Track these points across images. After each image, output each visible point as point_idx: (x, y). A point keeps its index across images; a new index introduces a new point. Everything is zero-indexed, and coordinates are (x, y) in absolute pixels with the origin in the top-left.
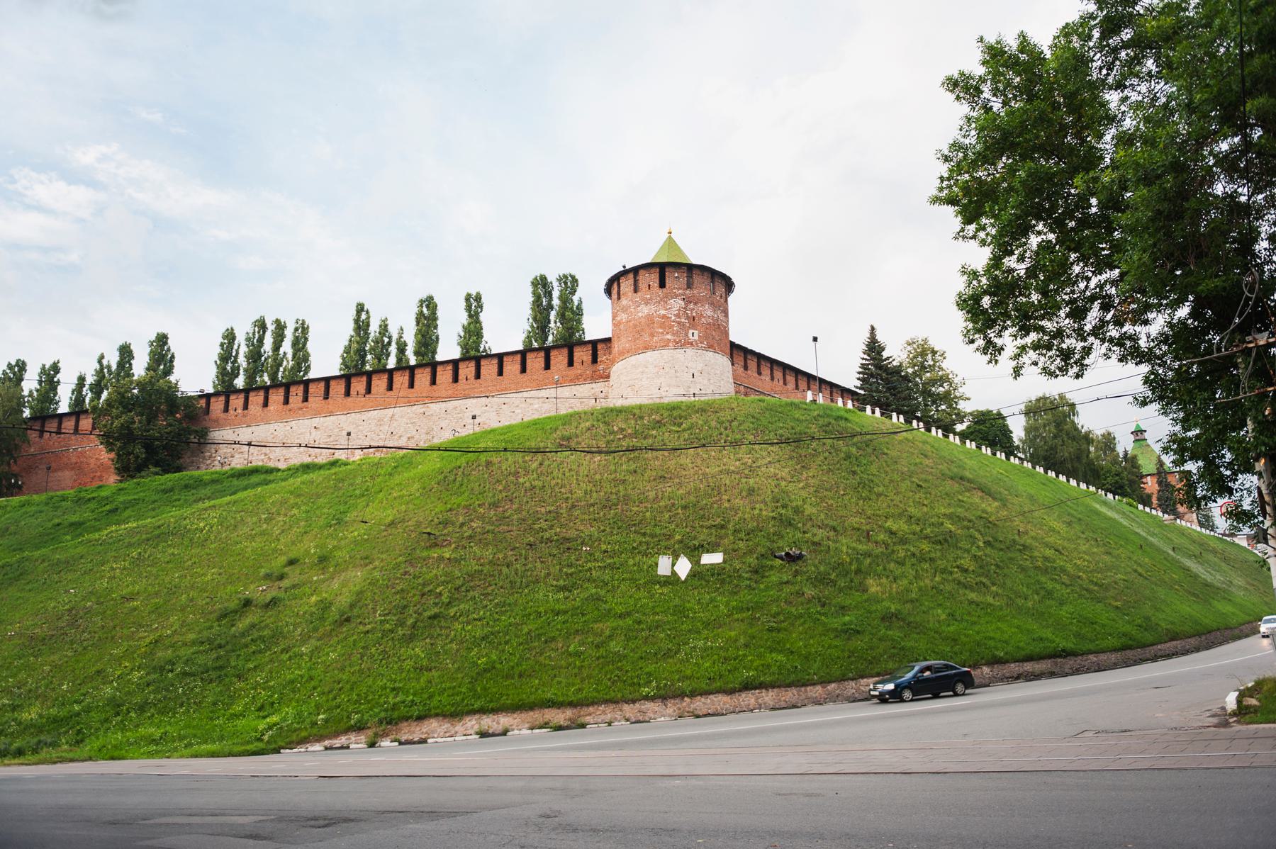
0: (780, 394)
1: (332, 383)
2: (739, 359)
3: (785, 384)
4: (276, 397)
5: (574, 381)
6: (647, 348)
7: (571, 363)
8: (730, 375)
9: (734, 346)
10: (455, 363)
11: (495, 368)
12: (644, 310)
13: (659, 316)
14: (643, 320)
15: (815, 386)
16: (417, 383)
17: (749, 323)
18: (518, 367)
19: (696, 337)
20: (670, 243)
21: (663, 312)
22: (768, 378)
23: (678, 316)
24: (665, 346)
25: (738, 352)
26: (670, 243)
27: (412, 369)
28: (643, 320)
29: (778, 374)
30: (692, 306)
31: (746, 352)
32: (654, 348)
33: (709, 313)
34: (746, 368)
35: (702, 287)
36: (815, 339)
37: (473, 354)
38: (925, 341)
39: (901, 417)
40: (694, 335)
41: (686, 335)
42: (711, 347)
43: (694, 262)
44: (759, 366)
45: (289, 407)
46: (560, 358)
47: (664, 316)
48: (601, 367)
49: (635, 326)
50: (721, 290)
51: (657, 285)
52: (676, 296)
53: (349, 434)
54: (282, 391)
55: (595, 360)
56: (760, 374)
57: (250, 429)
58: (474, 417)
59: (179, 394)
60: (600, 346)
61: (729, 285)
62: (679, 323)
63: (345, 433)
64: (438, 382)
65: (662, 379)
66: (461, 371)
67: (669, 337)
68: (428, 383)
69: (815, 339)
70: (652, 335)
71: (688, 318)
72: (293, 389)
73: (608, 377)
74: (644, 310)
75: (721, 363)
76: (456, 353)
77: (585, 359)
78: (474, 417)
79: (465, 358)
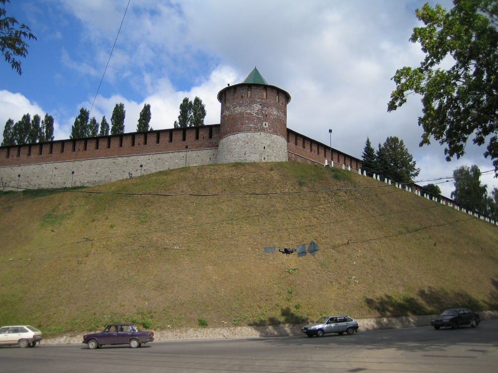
0: (309, 156)
1: (161, 135)
2: (292, 139)
3: (318, 153)
4: (35, 150)
5: (199, 147)
7: (197, 138)
8: (286, 148)
9: (289, 132)
10: (133, 135)
11: (168, 139)
13: (247, 113)
15: (329, 154)
16: (174, 139)
17: (295, 120)
19: (267, 126)
20: (256, 72)
21: (249, 111)
22: (309, 150)
23: (257, 114)
25: (291, 134)
27: (109, 138)
29: (315, 148)
30: (265, 108)
31: (297, 135)
33: (275, 113)
34: (296, 144)
35: (274, 99)
36: (330, 131)
39: (390, 181)
40: (266, 125)
42: (275, 132)
44: (304, 143)
45: (43, 155)
47: (250, 114)
50: (283, 100)
53: (73, 173)
54: (83, 143)
56: (304, 147)
57: (20, 168)
58: (141, 166)
59: (476, 118)
60: (214, 129)
61: (287, 97)
63: (71, 172)
64: (123, 145)
69: (330, 131)
72: (77, 145)
73: (218, 146)
75: (281, 141)
76: (134, 129)
77: (205, 135)
78: (141, 166)
79: (139, 133)
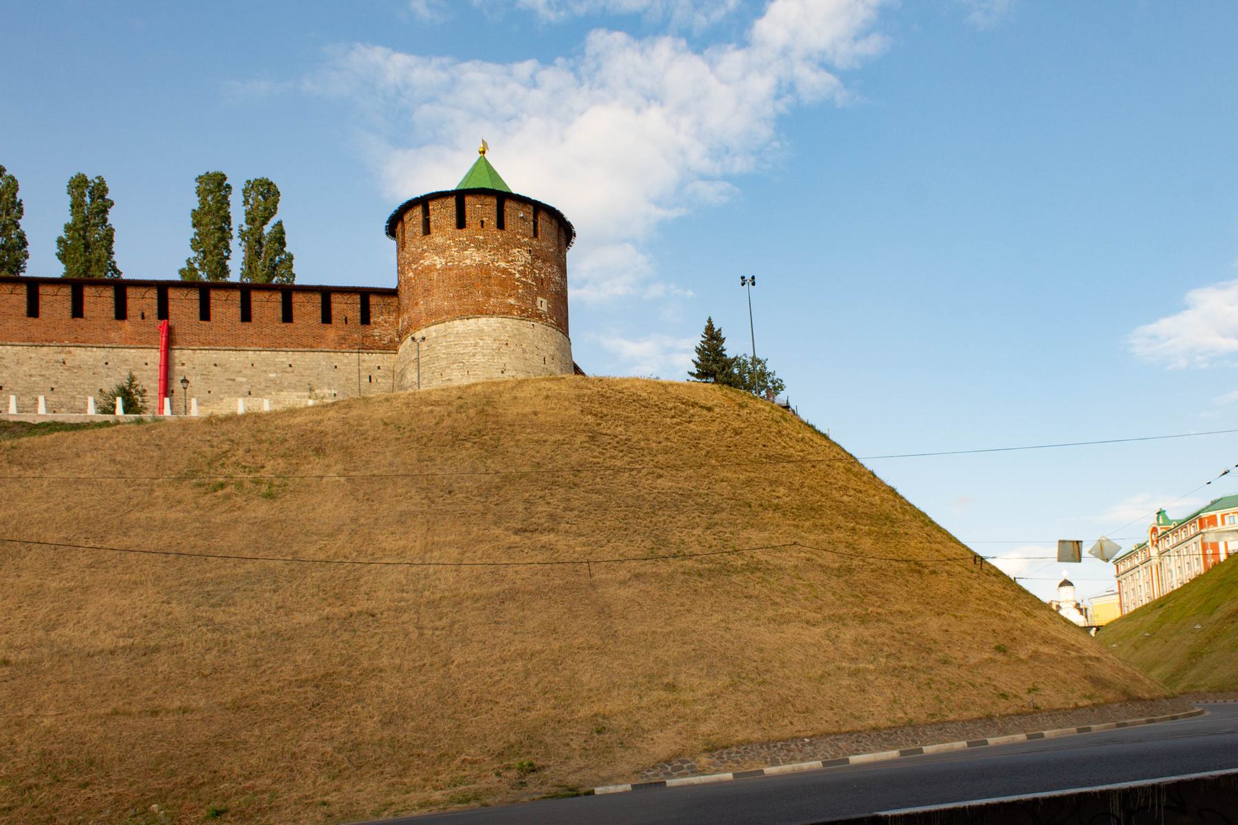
6: (480, 312)
12: (473, 257)
13: (497, 269)
14: (473, 272)
16: (44, 309)
18: (236, 311)
21: (503, 264)
23: (523, 273)
24: (507, 312)
26: (483, 165)
28: (473, 272)
32: (492, 314)
37: (91, 272)
38: (249, 182)
41: (534, 302)
43: (515, 190)
46: (310, 308)
47: (504, 271)
48: (376, 332)
49: (461, 277)
51: (493, 223)
52: (519, 245)
55: (365, 319)
61: (565, 231)
62: (525, 284)
65: (505, 360)
66: (130, 303)
67: (512, 301)
68: (68, 312)
70: (488, 295)
71: (535, 279)
74: (473, 257)
77: (350, 315)
